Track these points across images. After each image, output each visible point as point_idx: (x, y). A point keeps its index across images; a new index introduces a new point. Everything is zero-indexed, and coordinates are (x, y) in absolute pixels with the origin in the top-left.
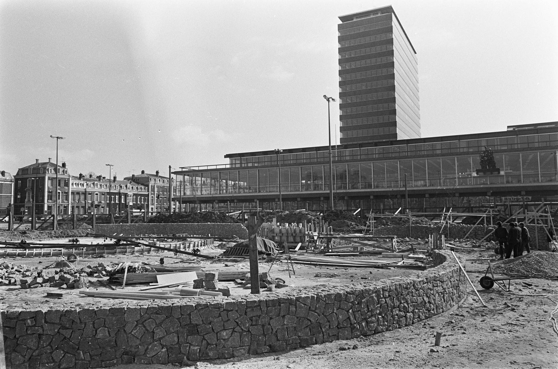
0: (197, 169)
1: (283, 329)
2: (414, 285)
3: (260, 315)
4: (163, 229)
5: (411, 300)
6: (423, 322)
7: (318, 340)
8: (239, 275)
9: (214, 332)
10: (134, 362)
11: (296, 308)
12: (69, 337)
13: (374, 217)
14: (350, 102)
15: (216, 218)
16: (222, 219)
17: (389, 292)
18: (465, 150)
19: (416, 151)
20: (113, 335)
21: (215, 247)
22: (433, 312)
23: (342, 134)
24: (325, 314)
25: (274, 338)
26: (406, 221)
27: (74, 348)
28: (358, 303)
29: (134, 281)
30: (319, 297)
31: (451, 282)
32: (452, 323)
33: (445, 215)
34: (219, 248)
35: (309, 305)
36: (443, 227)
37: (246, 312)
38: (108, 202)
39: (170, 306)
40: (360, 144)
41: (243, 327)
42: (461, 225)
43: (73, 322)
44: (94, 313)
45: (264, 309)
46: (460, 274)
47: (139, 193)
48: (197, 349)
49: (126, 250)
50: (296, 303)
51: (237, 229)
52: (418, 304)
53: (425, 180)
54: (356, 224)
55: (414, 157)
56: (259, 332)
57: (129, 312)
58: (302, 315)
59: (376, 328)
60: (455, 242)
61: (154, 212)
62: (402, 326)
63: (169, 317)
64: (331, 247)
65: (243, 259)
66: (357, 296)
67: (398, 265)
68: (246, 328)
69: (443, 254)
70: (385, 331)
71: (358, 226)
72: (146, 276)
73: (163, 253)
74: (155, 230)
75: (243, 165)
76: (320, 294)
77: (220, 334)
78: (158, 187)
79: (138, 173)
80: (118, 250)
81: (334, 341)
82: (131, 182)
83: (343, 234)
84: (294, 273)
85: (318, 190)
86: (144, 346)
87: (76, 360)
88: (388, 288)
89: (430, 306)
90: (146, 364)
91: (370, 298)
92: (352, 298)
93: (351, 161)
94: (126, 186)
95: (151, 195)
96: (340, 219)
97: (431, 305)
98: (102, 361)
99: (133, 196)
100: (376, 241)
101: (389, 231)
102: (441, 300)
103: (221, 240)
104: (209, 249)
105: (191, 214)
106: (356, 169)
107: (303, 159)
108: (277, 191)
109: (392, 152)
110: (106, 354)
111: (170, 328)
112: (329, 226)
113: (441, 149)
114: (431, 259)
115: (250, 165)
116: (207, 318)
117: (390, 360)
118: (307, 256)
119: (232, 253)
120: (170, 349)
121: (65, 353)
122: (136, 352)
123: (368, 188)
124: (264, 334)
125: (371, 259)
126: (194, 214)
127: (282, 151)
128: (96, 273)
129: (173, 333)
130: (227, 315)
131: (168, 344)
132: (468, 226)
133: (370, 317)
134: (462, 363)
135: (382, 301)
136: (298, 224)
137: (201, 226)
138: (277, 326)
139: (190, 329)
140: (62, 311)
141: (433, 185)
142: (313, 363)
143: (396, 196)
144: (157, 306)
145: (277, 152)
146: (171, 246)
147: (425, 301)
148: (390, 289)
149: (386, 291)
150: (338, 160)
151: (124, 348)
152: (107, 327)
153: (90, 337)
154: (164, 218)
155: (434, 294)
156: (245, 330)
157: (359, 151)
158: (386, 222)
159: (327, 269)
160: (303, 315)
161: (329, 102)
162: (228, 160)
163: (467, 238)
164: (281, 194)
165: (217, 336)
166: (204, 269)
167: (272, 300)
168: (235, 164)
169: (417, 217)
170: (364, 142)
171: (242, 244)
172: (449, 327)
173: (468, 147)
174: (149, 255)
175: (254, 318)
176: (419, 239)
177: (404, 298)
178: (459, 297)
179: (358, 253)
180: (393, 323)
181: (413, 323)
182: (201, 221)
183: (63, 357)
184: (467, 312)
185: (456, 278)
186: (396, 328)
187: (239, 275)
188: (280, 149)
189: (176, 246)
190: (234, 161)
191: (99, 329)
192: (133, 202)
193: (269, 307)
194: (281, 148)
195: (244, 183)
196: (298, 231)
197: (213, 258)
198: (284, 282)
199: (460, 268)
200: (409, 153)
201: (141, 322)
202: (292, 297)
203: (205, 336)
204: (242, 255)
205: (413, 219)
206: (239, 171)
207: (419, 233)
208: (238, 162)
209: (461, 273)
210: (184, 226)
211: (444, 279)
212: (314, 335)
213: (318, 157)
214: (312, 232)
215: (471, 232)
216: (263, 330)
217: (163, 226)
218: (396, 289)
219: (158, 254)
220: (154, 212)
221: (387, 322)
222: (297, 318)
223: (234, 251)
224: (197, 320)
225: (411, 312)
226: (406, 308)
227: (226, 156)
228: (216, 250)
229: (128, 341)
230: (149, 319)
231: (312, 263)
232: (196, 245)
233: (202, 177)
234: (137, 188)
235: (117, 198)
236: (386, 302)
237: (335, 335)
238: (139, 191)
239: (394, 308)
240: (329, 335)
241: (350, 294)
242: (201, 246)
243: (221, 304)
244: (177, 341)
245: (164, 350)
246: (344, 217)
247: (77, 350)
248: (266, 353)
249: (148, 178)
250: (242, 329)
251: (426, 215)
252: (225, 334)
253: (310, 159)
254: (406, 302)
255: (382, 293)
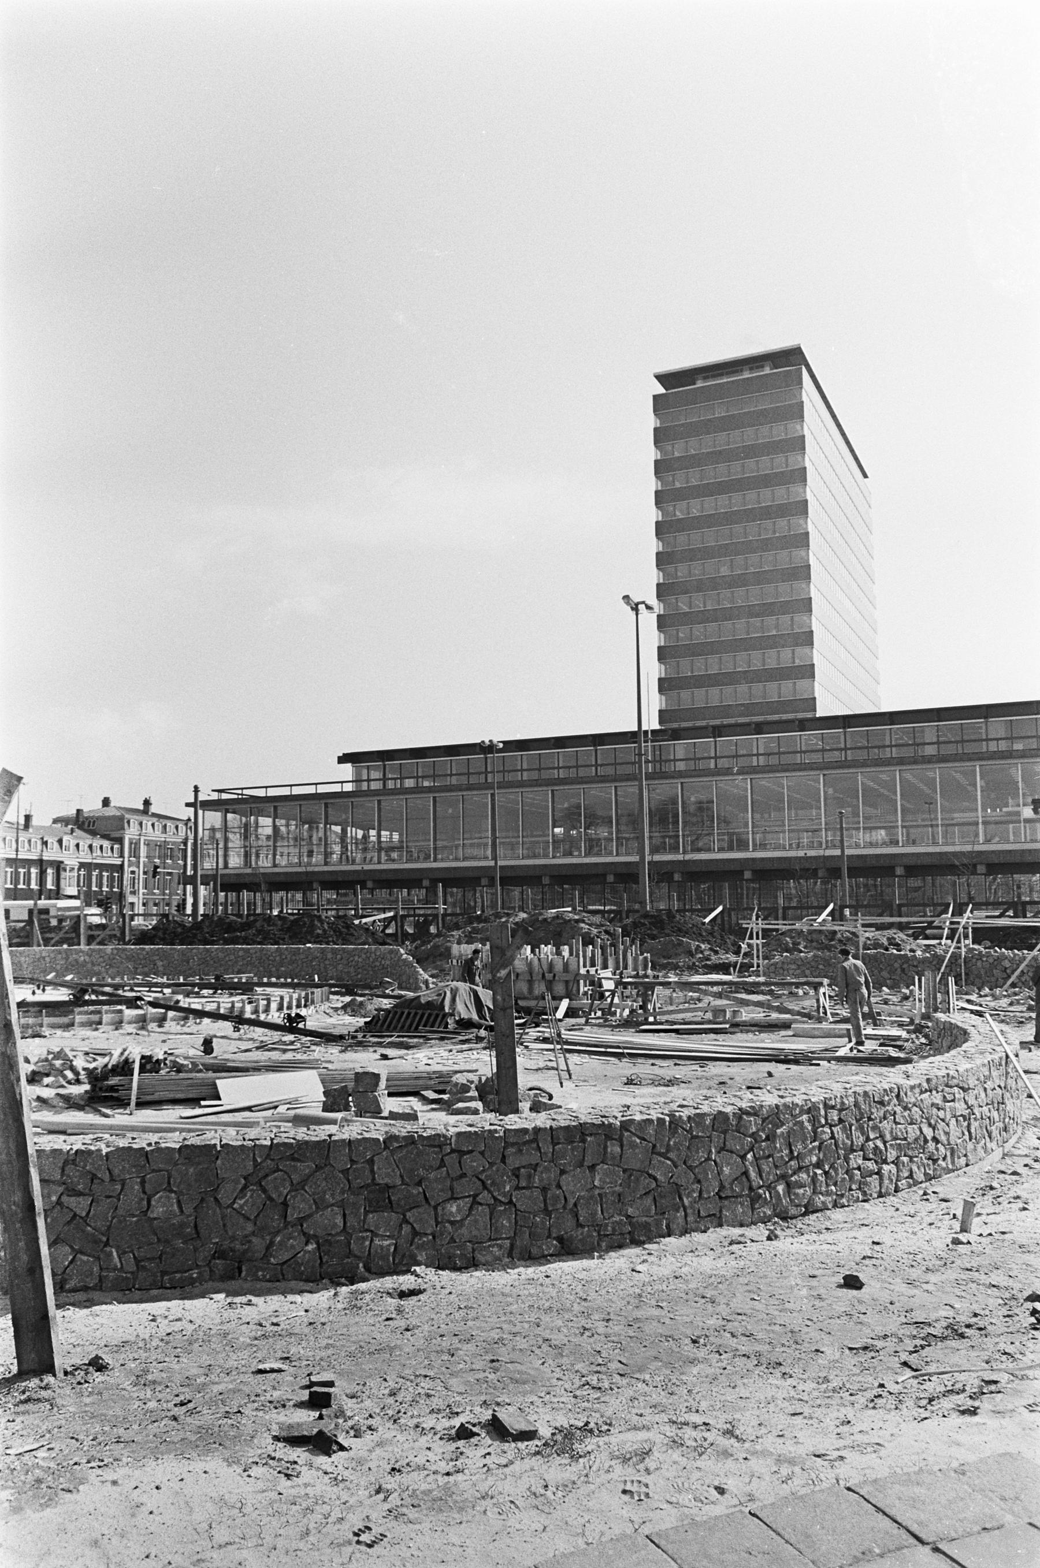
0: (261, 793)
1: (592, 1197)
2: (898, 1096)
3: (537, 1164)
4: (183, 961)
5: (891, 1132)
6: (920, 1188)
7: (674, 1226)
8: (431, 1079)
9: (429, 1204)
10: (240, 1275)
11: (622, 1146)
12: (84, 1214)
13: (763, 930)
14: (686, 609)
15: (324, 930)
16: (341, 933)
17: (840, 1111)
18: (1003, 746)
19: (867, 748)
20: (188, 1209)
21: (336, 1009)
22: (944, 1164)
23: (663, 698)
24: (689, 1163)
25: (569, 1223)
26: (848, 939)
27: (96, 1242)
28: (767, 1138)
29: (156, 1097)
30: (675, 1122)
31: (985, 1089)
32: (992, 1188)
33: (952, 923)
34: (346, 1012)
35: (653, 1139)
36: (948, 956)
37: (504, 1157)
38: (9, 886)
39: (325, 1140)
40: (714, 727)
41: (496, 1194)
42: (996, 951)
43: (92, 1180)
44: (143, 1158)
45: (547, 1148)
46: (1007, 1073)
47: (95, 861)
48: (389, 1245)
49: (101, 1018)
50: (621, 1136)
51: (388, 962)
52: (909, 1144)
53: (890, 829)
54: (711, 949)
55: (864, 764)
56: (535, 1204)
57: (227, 1154)
58: (635, 1165)
59: (810, 1200)
60: (981, 996)
61: (138, 915)
62: (871, 1195)
63: (322, 1168)
64: (654, 1009)
65: (421, 1040)
66: (764, 1120)
67: (838, 1054)
68: (504, 1195)
69: (960, 1024)
70: (830, 1206)
71: (716, 952)
72: (189, 1081)
73: (200, 1027)
74: (160, 963)
75: (390, 785)
76: (677, 1114)
77: (443, 1209)
78: (148, 844)
79: (92, 806)
80: (78, 1018)
81: (711, 1230)
82: (72, 831)
83: (677, 975)
84: (570, 1075)
85: (599, 854)
86: (263, 1238)
87: (101, 1269)
88: (838, 1100)
89: (937, 1149)
90: (269, 1281)
91: (795, 1125)
92: (753, 1124)
93: (693, 773)
94: (60, 841)
95: (129, 866)
96: (668, 935)
97: (939, 1145)
98: (164, 1273)
99: (79, 869)
100: (771, 992)
101: (803, 967)
102: (963, 1134)
103: (350, 992)
104: (318, 1016)
105: (255, 921)
106: (703, 797)
107: (558, 768)
108: (486, 858)
109: (803, 749)
110: (173, 1255)
111: (325, 1192)
112: (642, 954)
113: (938, 743)
114: (923, 1040)
115: (409, 783)
116: (412, 1170)
117: (864, 1258)
118: (591, 1033)
119: (389, 1026)
120: (324, 1244)
121: (76, 1252)
122: (245, 1251)
123: (739, 850)
124: (546, 1209)
125: (763, 1041)
126: (264, 920)
127: (501, 745)
128: (48, 1075)
129: (333, 1205)
130: (460, 1162)
131: (320, 1232)
132: (1015, 955)
133: (794, 1173)
134: (1027, 1265)
135: (825, 1133)
136: (558, 949)
137: (286, 953)
138: (578, 1191)
139: (371, 1196)
140: (68, 1152)
141: (914, 842)
142: (689, 1262)
143: (813, 873)
144: (292, 1141)
145: (485, 749)
146: (219, 1007)
147: (925, 1137)
148: (843, 1103)
149: (833, 1107)
150: (654, 773)
151: (217, 1243)
152: (175, 1192)
153: (134, 1216)
154: (179, 930)
155: (947, 1120)
156: (503, 1199)
157: (713, 747)
158: (793, 944)
159: (653, 1065)
160: (637, 1166)
161: (637, 615)
162: (347, 771)
163: (1013, 985)
164: (500, 863)
165: (436, 1215)
166: (330, 1066)
167: (565, 1127)
168: (369, 780)
169: (878, 929)
170: (726, 721)
171: (416, 1001)
172: (986, 1197)
173: (1011, 739)
174: (161, 1030)
175: (522, 1170)
176: (884, 988)
177: (875, 1128)
178: (1005, 1129)
179: (727, 1026)
180: (851, 1189)
181: (897, 1190)
182: (283, 939)
183: (71, 1262)
184: (1026, 1165)
185: (998, 1082)
186: (857, 1200)
187: (431, 1079)
188: (495, 741)
189: (233, 1006)
190: (365, 771)
191: (155, 1195)
192: (78, 885)
193: (559, 1143)
194: (498, 735)
195: (391, 835)
196: (559, 966)
197: (341, 1037)
198: (551, 1097)
199: (1007, 1057)
200: (849, 752)
201: (255, 1179)
202: (611, 1121)
203: (408, 1214)
204: (416, 1030)
205: (867, 935)
206: (379, 802)
207: (885, 974)
208: (375, 775)
209: (1010, 1070)
210: (241, 953)
211: (970, 1082)
212: (664, 1213)
213: (599, 762)
214: (597, 971)
215: (1022, 971)
216: (545, 1201)
217: (183, 953)
218: (856, 1104)
219: (186, 1030)
220: (138, 915)
221: (835, 1185)
222: (625, 1171)
223: (394, 1022)
224: (388, 1175)
225: (893, 1162)
226: (881, 1151)
227: (344, 759)
228: (341, 1017)
229: (224, 1225)
230: (275, 1172)
231: (609, 1050)
232: (285, 1005)
233: (275, 817)
234: (90, 847)
235: (33, 876)
236: (833, 1137)
237: (714, 1215)
238: (94, 854)
239: (853, 1151)
240: (699, 1216)
241: (748, 1114)
242: (298, 1006)
243: (444, 1136)
244: (342, 1225)
245: (311, 1247)
246: (680, 930)
247: (105, 1246)
248: (551, 1255)
249: (121, 818)
250: (495, 1199)
251: (900, 923)
252: (454, 1209)
253: (577, 767)
254: (881, 1136)
255: (823, 1112)
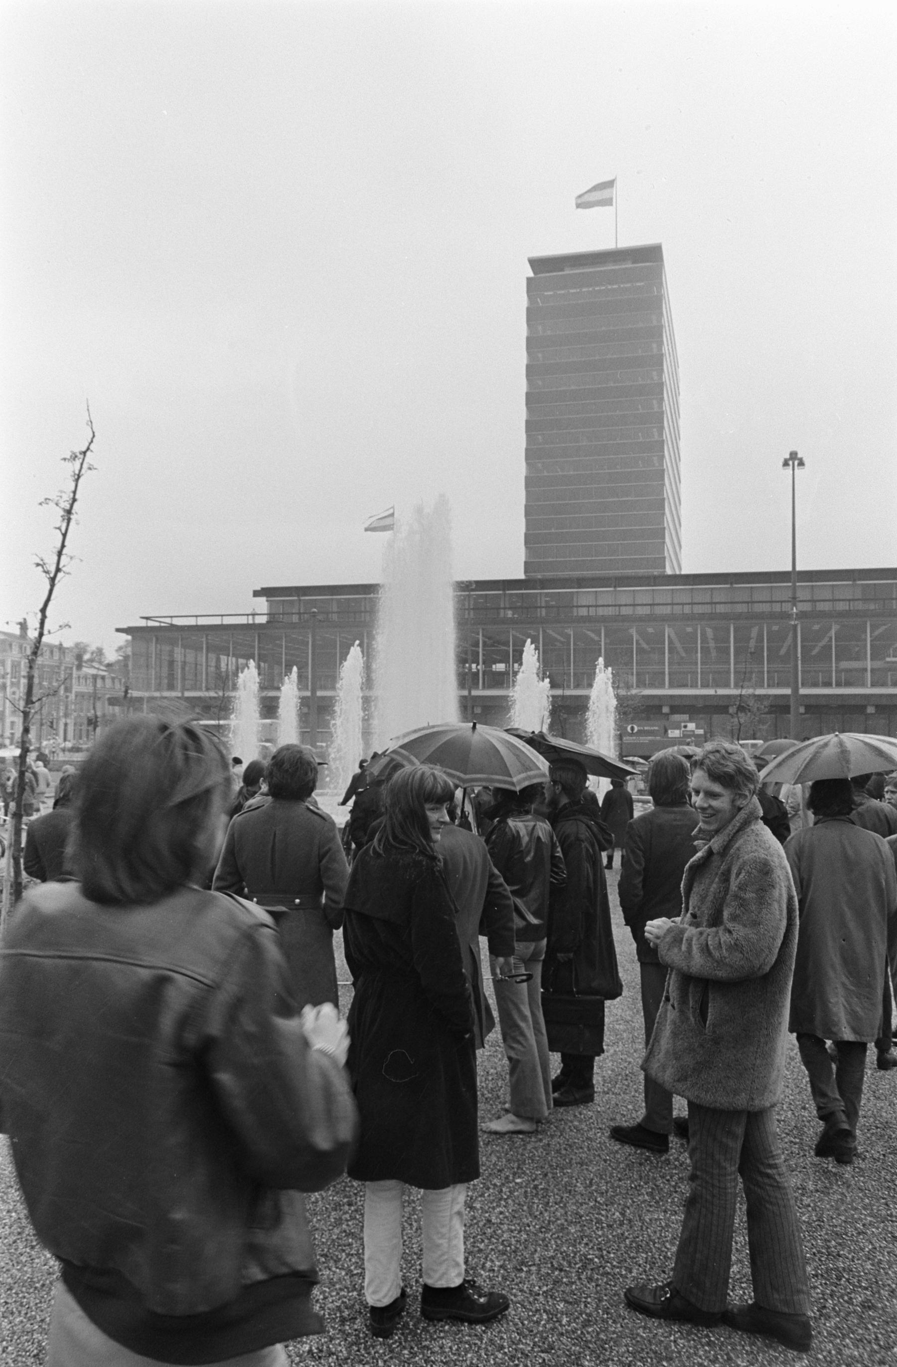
162: (262, 602)
227: (256, 594)
